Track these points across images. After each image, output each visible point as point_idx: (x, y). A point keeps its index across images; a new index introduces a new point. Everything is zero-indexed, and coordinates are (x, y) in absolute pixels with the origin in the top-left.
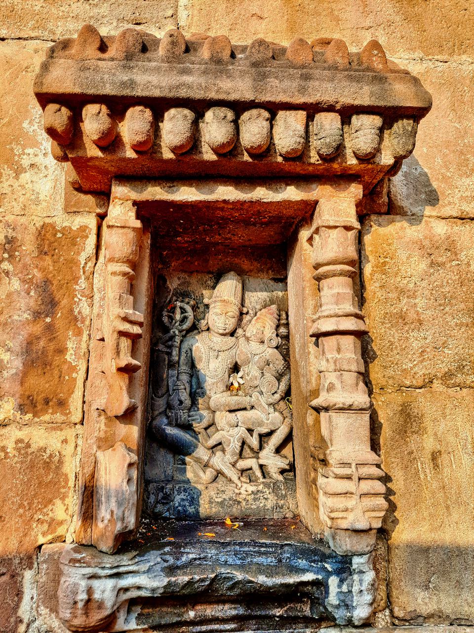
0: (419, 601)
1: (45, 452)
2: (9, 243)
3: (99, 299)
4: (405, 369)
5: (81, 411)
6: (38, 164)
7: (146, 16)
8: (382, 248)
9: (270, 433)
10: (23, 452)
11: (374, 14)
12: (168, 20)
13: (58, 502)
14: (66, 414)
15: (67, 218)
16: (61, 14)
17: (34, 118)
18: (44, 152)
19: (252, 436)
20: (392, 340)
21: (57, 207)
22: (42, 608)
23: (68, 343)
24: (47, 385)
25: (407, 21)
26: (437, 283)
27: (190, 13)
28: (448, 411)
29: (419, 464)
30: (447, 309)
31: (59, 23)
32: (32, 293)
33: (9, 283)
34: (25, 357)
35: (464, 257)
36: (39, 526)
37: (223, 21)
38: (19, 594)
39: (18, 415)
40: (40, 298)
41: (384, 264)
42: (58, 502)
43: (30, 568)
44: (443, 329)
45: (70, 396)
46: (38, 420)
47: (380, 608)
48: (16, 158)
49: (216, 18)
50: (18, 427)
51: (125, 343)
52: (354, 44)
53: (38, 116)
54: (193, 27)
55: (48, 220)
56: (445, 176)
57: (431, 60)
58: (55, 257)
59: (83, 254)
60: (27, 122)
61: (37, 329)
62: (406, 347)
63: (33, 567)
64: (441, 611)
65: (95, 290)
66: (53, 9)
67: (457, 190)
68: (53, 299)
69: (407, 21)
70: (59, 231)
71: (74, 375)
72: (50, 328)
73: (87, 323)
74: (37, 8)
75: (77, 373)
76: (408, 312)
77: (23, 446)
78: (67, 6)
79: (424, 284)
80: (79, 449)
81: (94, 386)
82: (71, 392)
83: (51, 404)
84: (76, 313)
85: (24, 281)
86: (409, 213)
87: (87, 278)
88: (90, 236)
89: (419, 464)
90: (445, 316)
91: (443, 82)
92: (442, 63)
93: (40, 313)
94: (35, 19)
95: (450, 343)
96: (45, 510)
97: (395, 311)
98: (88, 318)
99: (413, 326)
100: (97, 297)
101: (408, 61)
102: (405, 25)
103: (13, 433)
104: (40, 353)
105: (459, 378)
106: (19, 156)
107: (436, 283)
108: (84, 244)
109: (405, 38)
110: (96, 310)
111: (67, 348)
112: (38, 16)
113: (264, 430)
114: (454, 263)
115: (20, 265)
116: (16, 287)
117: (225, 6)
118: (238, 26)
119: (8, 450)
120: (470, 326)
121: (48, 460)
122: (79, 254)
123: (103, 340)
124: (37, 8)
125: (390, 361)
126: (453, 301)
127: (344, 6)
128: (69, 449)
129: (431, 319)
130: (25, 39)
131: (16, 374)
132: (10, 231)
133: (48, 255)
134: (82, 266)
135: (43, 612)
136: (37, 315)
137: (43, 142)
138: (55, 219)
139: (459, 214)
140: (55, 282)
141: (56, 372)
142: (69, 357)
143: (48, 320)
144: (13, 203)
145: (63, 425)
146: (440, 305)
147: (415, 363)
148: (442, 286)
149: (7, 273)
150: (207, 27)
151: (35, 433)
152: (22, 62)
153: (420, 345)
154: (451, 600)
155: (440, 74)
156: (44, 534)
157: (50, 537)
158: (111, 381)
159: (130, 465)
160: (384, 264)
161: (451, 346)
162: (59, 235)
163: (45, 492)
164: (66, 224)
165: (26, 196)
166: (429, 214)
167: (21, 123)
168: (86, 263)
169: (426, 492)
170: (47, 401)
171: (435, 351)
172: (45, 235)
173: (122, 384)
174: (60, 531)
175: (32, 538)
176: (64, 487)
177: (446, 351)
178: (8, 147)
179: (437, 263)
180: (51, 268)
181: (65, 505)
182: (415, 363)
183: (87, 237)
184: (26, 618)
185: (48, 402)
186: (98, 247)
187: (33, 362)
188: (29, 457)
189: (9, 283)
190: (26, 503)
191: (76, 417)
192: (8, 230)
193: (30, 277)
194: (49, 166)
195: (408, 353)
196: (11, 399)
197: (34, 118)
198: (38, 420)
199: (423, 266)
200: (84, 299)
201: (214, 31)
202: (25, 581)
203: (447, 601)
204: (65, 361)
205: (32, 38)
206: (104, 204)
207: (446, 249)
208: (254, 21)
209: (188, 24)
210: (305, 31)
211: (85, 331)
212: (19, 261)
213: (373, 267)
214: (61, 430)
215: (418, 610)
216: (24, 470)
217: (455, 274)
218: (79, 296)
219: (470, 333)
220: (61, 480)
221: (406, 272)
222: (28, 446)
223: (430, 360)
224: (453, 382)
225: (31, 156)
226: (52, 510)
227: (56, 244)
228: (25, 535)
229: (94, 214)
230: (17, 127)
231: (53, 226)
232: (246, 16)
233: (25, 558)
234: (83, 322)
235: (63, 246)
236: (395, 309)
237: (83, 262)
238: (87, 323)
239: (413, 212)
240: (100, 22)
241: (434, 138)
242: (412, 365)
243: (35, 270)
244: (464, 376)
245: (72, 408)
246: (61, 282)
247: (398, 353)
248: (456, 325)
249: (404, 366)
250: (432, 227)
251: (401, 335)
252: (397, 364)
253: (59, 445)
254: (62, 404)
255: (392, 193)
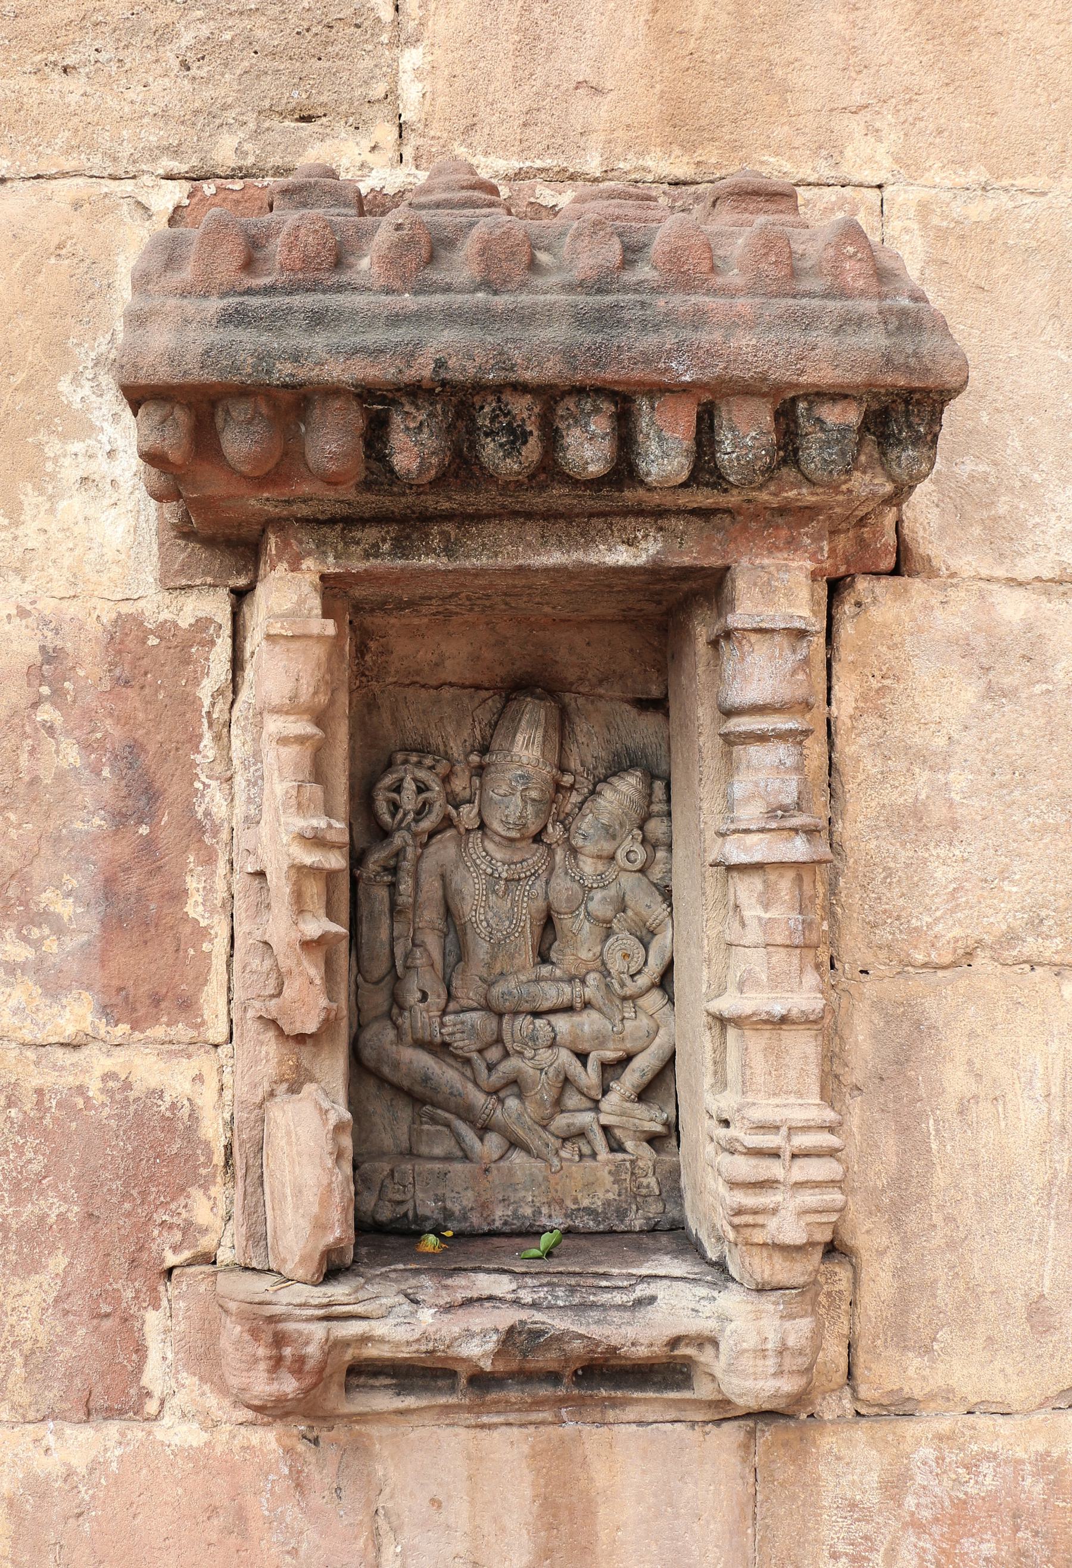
0: (911, 1372)
1: (161, 1097)
2: (49, 663)
3: (244, 784)
4: (916, 929)
5: (226, 1019)
6: (96, 477)
7: (323, 98)
8: (878, 656)
9: (625, 1061)
10: (118, 1097)
11: (872, 71)
12: (376, 107)
13: (196, 1192)
14: (197, 1026)
15: (167, 601)
16: (127, 109)
17: (81, 369)
18: (108, 448)
19: (584, 1065)
20: (892, 865)
21: (143, 576)
22: (185, 1374)
23: (188, 879)
24: (153, 967)
25: (952, 89)
26: (999, 735)
27: (428, 88)
28: (1000, 1015)
29: (931, 1122)
30: (1016, 793)
31: (124, 132)
32: (106, 772)
33: (57, 752)
34: (102, 908)
35: (1061, 675)
36: (165, 1234)
37: (506, 104)
38: (141, 1350)
39: (103, 1028)
40: (123, 783)
41: (882, 691)
42: (196, 1192)
43: (156, 1307)
44: (1003, 839)
45: (200, 991)
46: (142, 1036)
47: (832, 1386)
48: (49, 467)
49: (490, 98)
50: (104, 1050)
51: (314, 890)
52: (824, 153)
53: (90, 364)
54: (435, 124)
55: (126, 608)
56: (1027, 481)
57: (1006, 190)
58: (147, 691)
59: (205, 682)
60: (68, 378)
61: (123, 850)
62: (921, 879)
63: (159, 1306)
64: (951, 1390)
65: (236, 762)
66: (109, 98)
67: (1053, 516)
68: (150, 785)
69: (952, 89)
70: (152, 632)
71: (206, 947)
72: (148, 845)
73: (224, 835)
74: (73, 99)
75: (211, 941)
76: (930, 802)
77: (119, 1086)
78: (140, 88)
79: (968, 738)
80: (227, 1095)
81: (248, 970)
82: (202, 979)
83: (163, 1005)
84: (200, 815)
85: (86, 747)
86: (944, 572)
87: (217, 738)
88: (219, 641)
89: (931, 1122)
90: (1009, 811)
91: (1034, 244)
92: (1032, 198)
93: (125, 816)
94: (70, 125)
95: (1016, 870)
96: (173, 1206)
97: (901, 801)
98: (226, 825)
99: (938, 835)
100: (239, 781)
101: (950, 195)
102: (948, 99)
103: (94, 1060)
104: (132, 899)
105: (1031, 946)
106: (55, 460)
107: (994, 736)
108: (207, 659)
109: (946, 134)
110: (240, 811)
111: (186, 891)
112: (76, 119)
113: (610, 1055)
114: (1038, 689)
115: (76, 711)
116: (72, 760)
117: (511, 64)
118: (542, 116)
119: (91, 1094)
120: (1062, 830)
121: (168, 1114)
122: (196, 682)
123: (261, 874)
124: (73, 99)
125: (885, 911)
126: (1031, 777)
127: (799, 54)
128: (207, 1097)
129: (979, 818)
130: (51, 177)
131: (89, 943)
132: (50, 634)
133: (132, 687)
134: (205, 710)
135: (187, 1382)
136: (120, 819)
137: (105, 425)
138: (141, 604)
139: (1055, 573)
140: (152, 748)
141: (168, 940)
142: (194, 908)
143: (144, 830)
144: (51, 571)
145: (191, 1047)
146: (1002, 786)
147: (938, 914)
148: (1008, 743)
149: (50, 730)
150: (470, 121)
151: (137, 1061)
152: (47, 235)
153: (950, 876)
154: (973, 1370)
155: (1028, 226)
156: (175, 1249)
157: (186, 1254)
158: (285, 963)
159: (339, 1128)
160: (882, 691)
161: (1017, 877)
162: (153, 641)
163: (169, 1173)
164: (165, 615)
165: (76, 553)
166: (988, 572)
167: (55, 380)
168: (213, 704)
169: (941, 1175)
170: (156, 1001)
171: (983, 888)
172: (122, 642)
173: (313, 972)
174: (206, 1243)
175: (154, 1254)
176: (205, 1165)
177: (1007, 886)
178: (30, 440)
179: (1002, 690)
180: (141, 716)
181: (209, 1198)
182: (938, 914)
183: (213, 643)
184: (157, 1390)
185: (159, 1001)
186: (237, 663)
187: (120, 921)
188: (132, 1108)
189: (57, 752)
190: (135, 1192)
191: (218, 1031)
192: (45, 631)
193: (99, 735)
194: (121, 480)
195: (924, 894)
196: (86, 995)
197: (81, 369)
198: (142, 1036)
199: (970, 693)
200: (214, 784)
201: (486, 131)
202: (147, 1328)
203: (965, 1372)
204: (185, 918)
205: (65, 175)
206: (245, 566)
207: (1023, 657)
208: (582, 101)
209: (423, 116)
210: (704, 122)
211: (220, 854)
212: (74, 702)
213: (856, 700)
214: (189, 1057)
215: (906, 1389)
216: (125, 1132)
217: (1039, 713)
218: (203, 778)
219: (1062, 845)
220: (199, 1152)
221: (931, 710)
222: (127, 1086)
223: (971, 908)
224: (1015, 953)
225: (80, 459)
226: (185, 1206)
227: (145, 662)
228: (141, 1249)
229: (226, 591)
230: (46, 392)
231: (137, 620)
232: (563, 88)
233: (144, 1289)
234: (215, 833)
235: (163, 665)
236: (901, 795)
237: (207, 702)
238: (224, 835)
239: (953, 569)
240: (218, 121)
241: (1008, 388)
242: (930, 920)
243: (108, 721)
244: (1040, 940)
245: (207, 1014)
246: (166, 746)
247: (903, 895)
248: (1033, 831)
249: (914, 921)
250: (992, 604)
251: (911, 853)
252: (898, 918)
253: (187, 1086)
254: (187, 1006)
255: (905, 524)
